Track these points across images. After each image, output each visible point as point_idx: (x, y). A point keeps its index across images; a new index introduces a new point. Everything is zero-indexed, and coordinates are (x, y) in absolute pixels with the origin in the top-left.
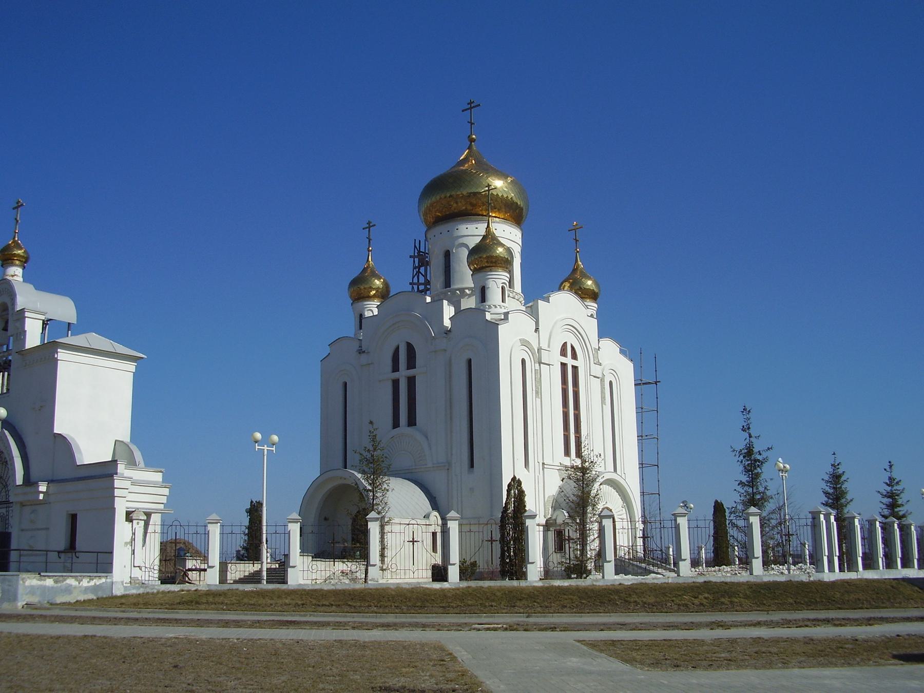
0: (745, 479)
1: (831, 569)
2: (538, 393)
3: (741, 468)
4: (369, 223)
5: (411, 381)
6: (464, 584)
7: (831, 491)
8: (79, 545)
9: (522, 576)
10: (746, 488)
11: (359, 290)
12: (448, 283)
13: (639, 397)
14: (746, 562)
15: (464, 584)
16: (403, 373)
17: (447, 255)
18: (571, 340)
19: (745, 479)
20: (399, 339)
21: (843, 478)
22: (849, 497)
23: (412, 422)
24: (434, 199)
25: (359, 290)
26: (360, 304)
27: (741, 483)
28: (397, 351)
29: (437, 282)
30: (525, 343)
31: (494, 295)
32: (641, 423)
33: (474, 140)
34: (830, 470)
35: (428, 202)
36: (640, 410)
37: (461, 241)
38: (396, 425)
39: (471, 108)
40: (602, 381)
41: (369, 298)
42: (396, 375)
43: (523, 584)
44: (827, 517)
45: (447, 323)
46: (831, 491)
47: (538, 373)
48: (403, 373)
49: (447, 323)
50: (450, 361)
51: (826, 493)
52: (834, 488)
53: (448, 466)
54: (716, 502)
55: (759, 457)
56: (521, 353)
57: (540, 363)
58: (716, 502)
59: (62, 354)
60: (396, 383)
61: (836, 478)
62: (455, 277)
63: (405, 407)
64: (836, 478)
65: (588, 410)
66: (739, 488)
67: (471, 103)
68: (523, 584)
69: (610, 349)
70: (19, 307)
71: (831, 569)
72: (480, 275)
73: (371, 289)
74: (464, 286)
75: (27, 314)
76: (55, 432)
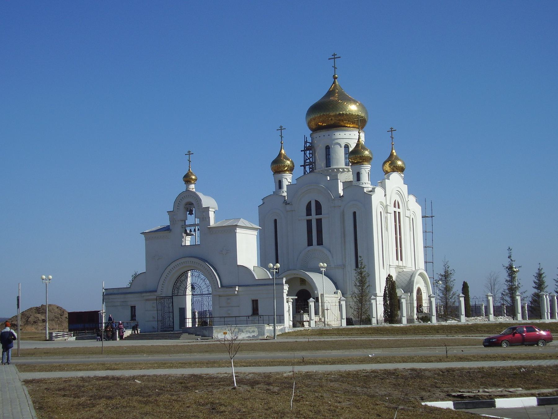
0: (508, 279)
1: (548, 318)
2: (387, 229)
3: (507, 274)
4: (281, 127)
5: (319, 222)
6: (409, 325)
7: (537, 281)
8: (260, 312)
9: (400, 322)
10: (509, 283)
11: (278, 166)
12: (328, 163)
13: (425, 225)
14: (487, 314)
15: (409, 325)
16: (314, 217)
17: (328, 148)
18: (398, 199)
19: (508, 279)
20: (312, 197)
21: (543, 276)
22: (546, 284)
23: (320, 243)
24: (316, 116)
25: (278, 166)
26: (280, 175)
27: (507, 281)
28: (309, 204)
29: (321, 163)
30: (381, 203)
31: (365, 178)
32: (425, 240)
33: (336, 78)
34: (537, 271)
35: (313, 116)
36: (425, 232)
37: (338, 141)
38: (310, 243)
39: (334, 58)
40: (410, 218)
41: (284, 171)
42: (309, 218)
43: (402, 325)
44: (546, 297)
45: (341, 192)
46: (537, 281)
47: (386, 218)
48: (314, 217)
49: (341, 192)
50: (343, 211)
51: (535, 282)
52: (539, 280)
53: (343, 266)
54: (464, 282)
55: (515, 270)
56: (380, 209)
57: (387, 213)
58: (464, 282)
59: (238, 230)
60: (309, 222)
61: (540, 275)
62: (333, 161)
63: (315, 234)
64: (540, 275)
65: (404, 235)
66: (506, 283)
67: (334, 55)
68: (542, 321)
69: (412, 199)
70: (204, 206)
71: (548, 318)
72: (356, 166)
73: (284, 167)
74: (339, 167)
75: (210, 209)
76: (239, 263)
